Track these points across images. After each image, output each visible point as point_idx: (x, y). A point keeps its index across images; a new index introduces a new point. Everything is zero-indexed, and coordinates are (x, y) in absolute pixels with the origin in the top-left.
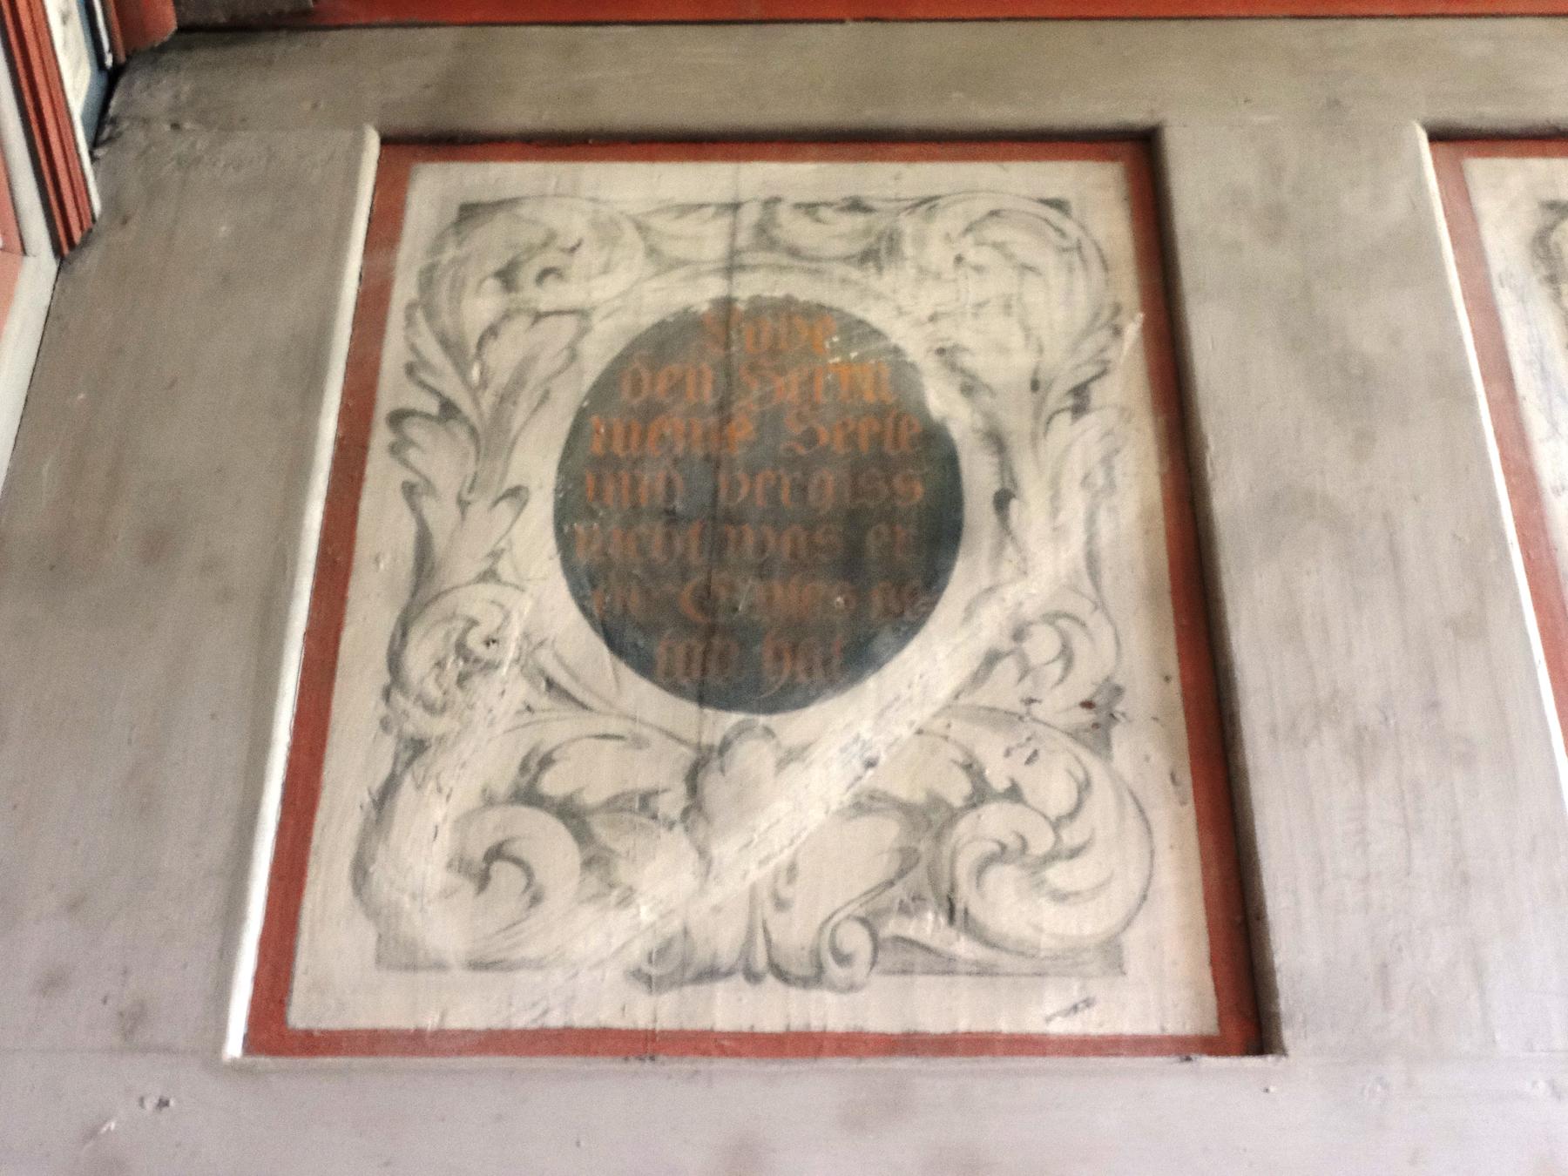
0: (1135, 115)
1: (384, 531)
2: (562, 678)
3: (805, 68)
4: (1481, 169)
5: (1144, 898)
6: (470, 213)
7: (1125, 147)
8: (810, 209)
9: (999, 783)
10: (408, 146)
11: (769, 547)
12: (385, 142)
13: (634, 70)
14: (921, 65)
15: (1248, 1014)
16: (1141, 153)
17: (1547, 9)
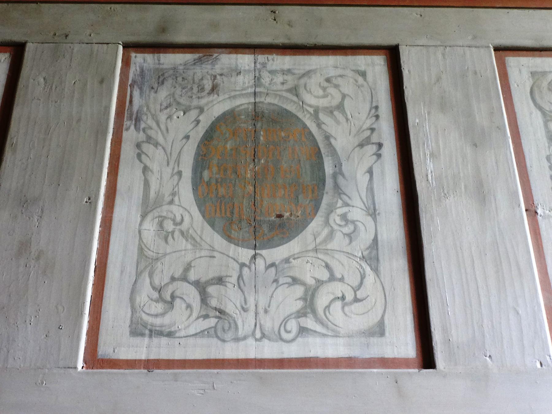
0: (18, 38)
3: (296, 23)
4: (514, 62)
15: (427, 359)
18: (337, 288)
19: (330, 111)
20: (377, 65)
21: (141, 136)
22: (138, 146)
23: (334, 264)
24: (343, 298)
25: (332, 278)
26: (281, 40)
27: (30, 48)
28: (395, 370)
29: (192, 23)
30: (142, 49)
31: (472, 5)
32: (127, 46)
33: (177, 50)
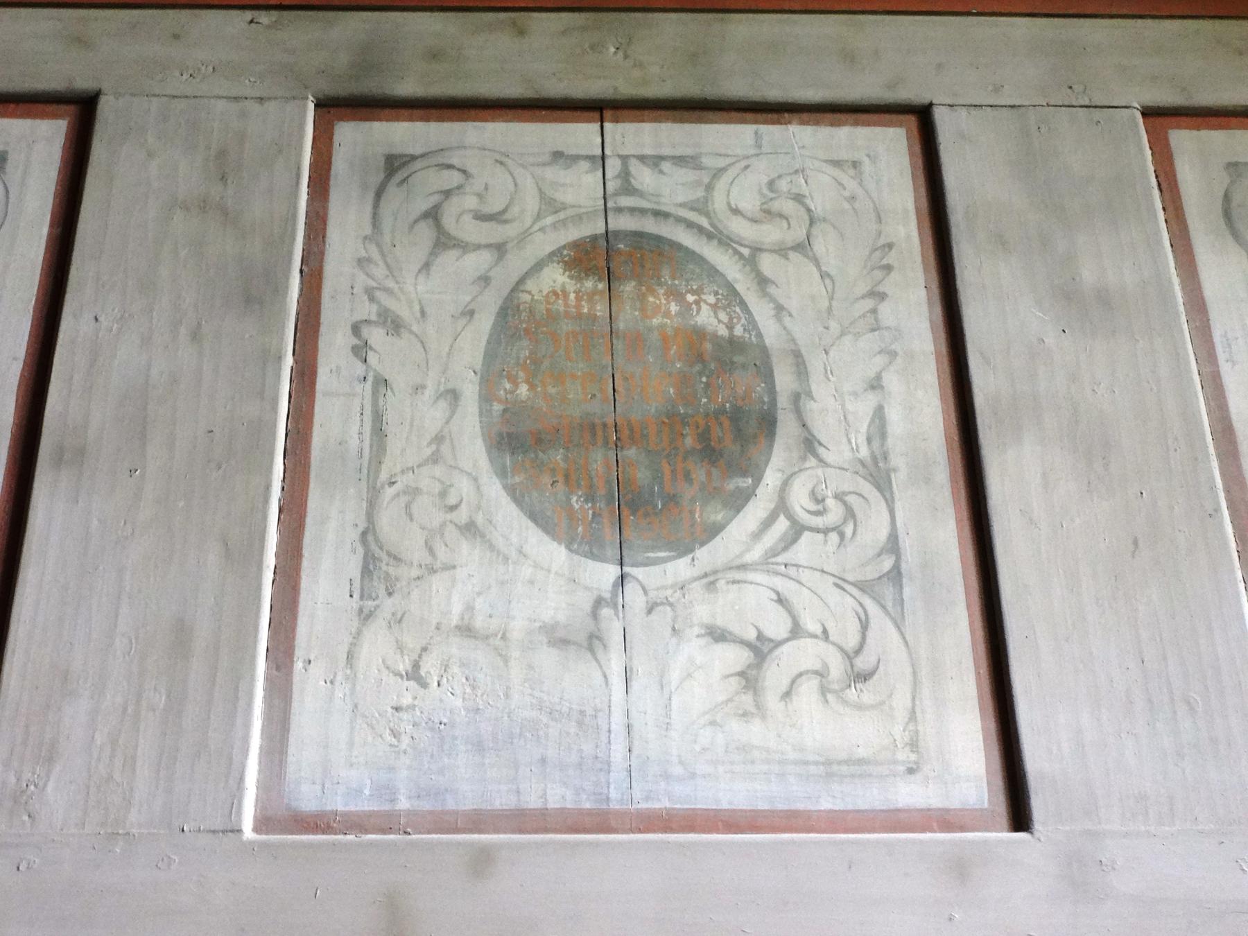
0: (83, 83)
1: (337, 420)
2: (738, 575)
3: (656, 51)
4: (1182, 140)
5: (605, 677)
6: (395, 165)
7: (71, 109)
8: (654, 161)
9: (812, 626)
10: (335, 107)
11: (647, 440)
12: (318, 106)
13: (493, 53)
14: (750, 50)
15: (1020, 818)
16: (922, 119)
17: (1024, 10)
18: (805, 654)
19: (781, 251)
20: (891, 146)
21: (367, 310)
22: (356, 329)
23: (801, 599)
24: (821, 674)
25: (796, 631)
26: (513, 89)
27: (106, 107)
28: (704, 836)
29: (422, 49)
30: (638, 113)
31: (823, 8)
32: (323, 105)
33: (710, 115)
